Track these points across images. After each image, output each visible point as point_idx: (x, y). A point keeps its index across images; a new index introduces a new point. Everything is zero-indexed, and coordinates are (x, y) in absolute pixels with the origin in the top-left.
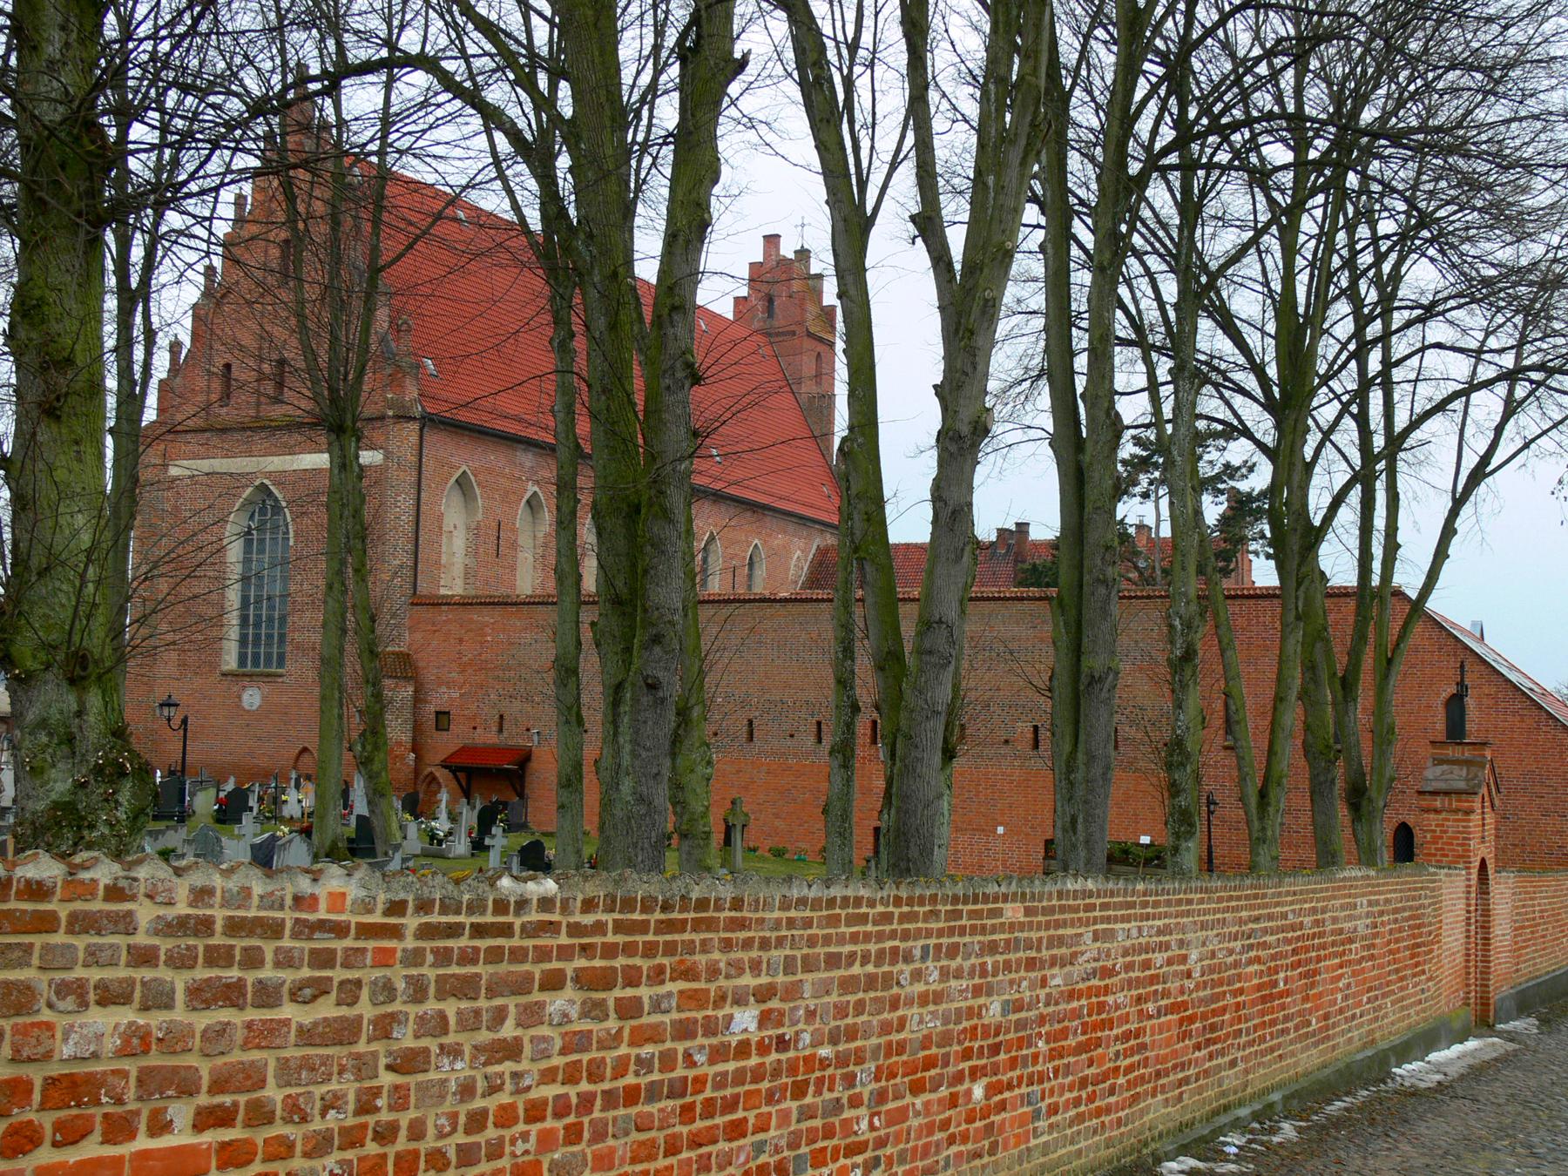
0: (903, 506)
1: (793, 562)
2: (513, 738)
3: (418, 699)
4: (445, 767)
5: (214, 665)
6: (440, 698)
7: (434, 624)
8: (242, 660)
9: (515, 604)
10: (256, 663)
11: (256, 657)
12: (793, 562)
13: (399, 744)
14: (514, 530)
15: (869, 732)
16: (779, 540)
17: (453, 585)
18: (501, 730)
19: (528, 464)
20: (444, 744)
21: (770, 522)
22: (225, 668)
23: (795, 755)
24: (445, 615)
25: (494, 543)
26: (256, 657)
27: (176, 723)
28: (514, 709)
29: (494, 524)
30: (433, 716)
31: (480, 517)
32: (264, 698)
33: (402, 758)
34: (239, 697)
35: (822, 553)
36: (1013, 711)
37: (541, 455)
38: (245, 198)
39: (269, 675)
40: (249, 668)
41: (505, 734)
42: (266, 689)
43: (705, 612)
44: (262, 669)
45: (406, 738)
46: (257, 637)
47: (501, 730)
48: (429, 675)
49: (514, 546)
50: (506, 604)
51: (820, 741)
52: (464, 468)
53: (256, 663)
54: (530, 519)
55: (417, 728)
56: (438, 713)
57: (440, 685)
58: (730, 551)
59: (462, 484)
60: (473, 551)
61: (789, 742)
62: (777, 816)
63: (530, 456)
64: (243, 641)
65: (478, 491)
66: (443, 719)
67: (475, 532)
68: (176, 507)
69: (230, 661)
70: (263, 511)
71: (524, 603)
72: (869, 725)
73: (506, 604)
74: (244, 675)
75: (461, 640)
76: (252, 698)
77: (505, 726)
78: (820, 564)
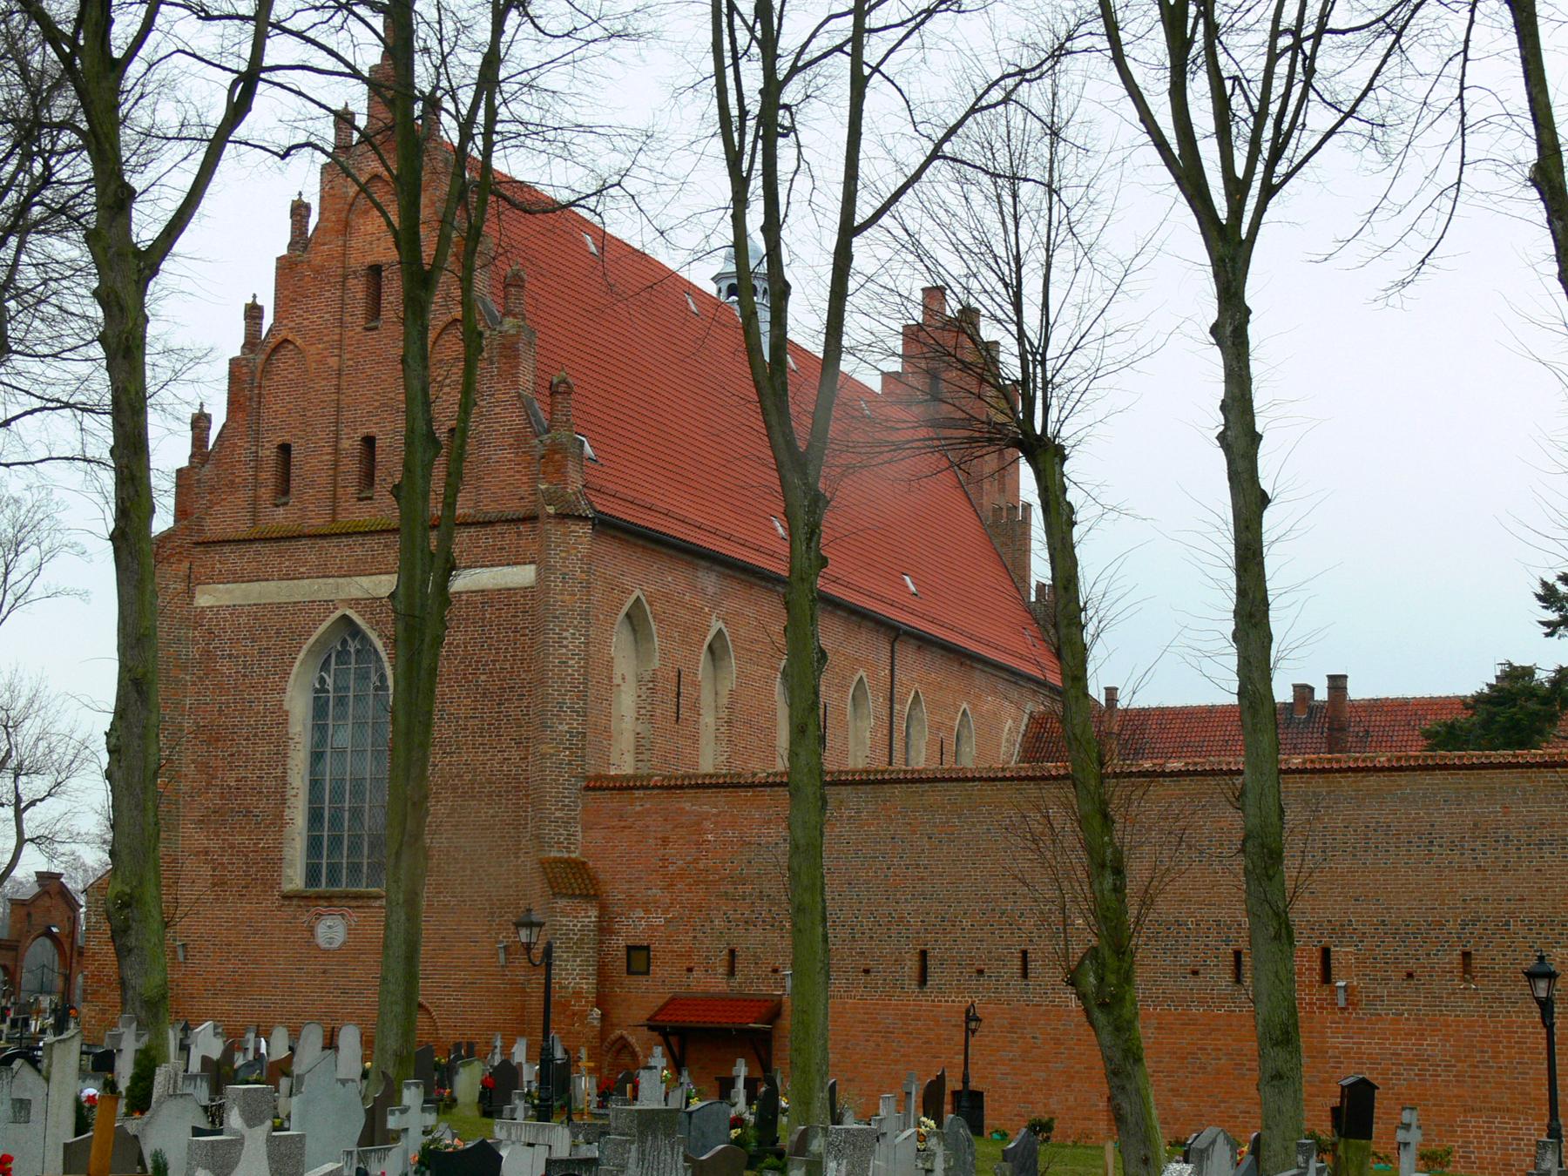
0: (1098, 662)
1: (1005, 735)
2: (753, 982)
3: (604, 928)
4: (651, 1028)
5: (271, 883)
6: (635, 926)
7: (621, 818)
8: (312, 874)
9: (752, 786)
10: (333, 879)
11: (334, 870)
12: (1005, 735)
13: (578, 994)
14: (696, 685)
15: (1317, 965)
16: (990, 703)
17: (624, 764)
18: (731, 972)
19: (711, 590)
20: (644, 996)
21: (979, 678)
22: (288, 887)
23: (1202, 1002)
24: (639, 804)
25: (672, 700)
26: (334, 870)
27: (538, 952)
28: (750, 941)
29: (673, 674)
30: (622, 954)
31: (656, 664)
32: (349, 930)
33: (583, 1016)
34: (312, 930)
35: (1037, 722)
36: (1546, 930)
37: (726, 577)
38: (308, 207)
39: (357, 897)
40: (323, 887)
41: (739, 978)
42: (355, 917)
43: (847, 803)
44: (343, 887)
45: (588, 986)
46: (336, 841)
47: (731, 972)
48: (617, 893)
49: (695, 708)
50: (737, 786)
51: (1238, 979)
52: (638, 592)
53: (333, 879)
54: (710, 668)
55: (603, 974)
56: (630, 949)
57: (632, 908)
58: (937, 718)
59: (635, 619)
60: (646, 713)
61: (1191, 982)
62: (1175, 1092)
63: (713, 577)
64: (314, 845)
65: (654, 628)
66: (639, 957)
67: (649, 686)
68: (207, 654)
69: (295, 877)
70: (343, 655)
71: (766, 785)
72: (1317, 954)
73: (737, 786)
74: (319, 897)
75: (665, 841)
76: (331, 931)
77: (739, 967)
78: (1038, 738)
